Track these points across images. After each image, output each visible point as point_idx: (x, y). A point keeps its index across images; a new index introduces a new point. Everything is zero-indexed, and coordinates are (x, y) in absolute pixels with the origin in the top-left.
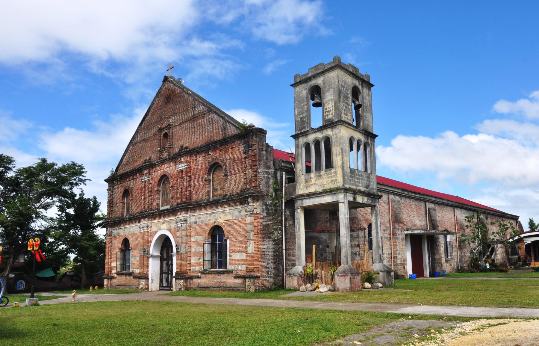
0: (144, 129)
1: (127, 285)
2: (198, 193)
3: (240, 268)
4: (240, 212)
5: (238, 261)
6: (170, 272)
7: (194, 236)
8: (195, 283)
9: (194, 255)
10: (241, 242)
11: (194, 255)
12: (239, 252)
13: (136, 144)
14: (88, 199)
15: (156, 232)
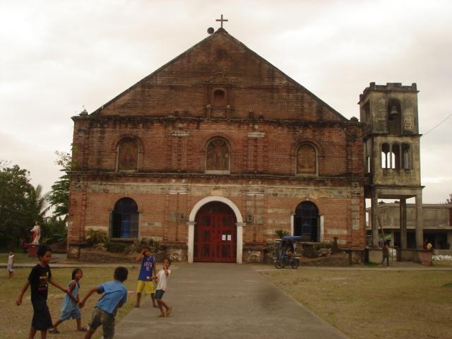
4: (340, 193)
7: (272, 208)
15: (202, 197)
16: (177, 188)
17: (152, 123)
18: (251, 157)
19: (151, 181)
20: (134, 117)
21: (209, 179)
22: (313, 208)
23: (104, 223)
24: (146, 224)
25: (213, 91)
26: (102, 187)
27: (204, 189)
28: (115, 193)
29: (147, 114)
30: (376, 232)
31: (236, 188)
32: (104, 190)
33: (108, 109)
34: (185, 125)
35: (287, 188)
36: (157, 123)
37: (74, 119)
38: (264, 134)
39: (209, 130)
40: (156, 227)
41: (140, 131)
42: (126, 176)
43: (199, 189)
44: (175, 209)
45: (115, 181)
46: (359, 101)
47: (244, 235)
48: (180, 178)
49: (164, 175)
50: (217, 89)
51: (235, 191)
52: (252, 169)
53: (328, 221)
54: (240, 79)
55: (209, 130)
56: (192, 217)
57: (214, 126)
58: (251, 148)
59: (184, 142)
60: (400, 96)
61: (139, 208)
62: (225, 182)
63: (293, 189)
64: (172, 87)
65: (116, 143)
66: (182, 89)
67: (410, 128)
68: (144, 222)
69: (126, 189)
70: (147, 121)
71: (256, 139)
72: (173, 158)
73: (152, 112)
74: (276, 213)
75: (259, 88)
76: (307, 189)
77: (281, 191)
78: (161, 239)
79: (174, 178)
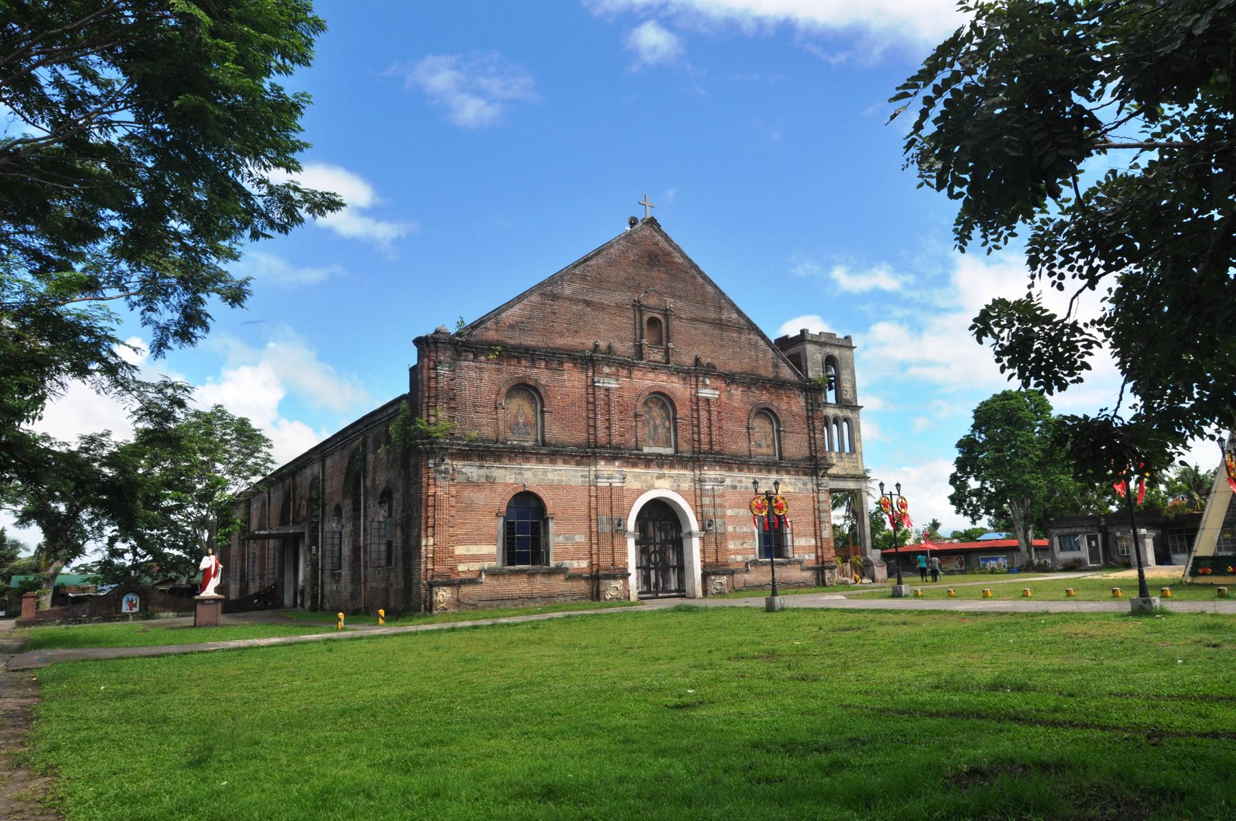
0: (584, 278)
1: (535, 595)
2: (736, 443)
3: (807, 557)
4: (805, 484)
5: (803, 548)
6: (652, 566)
7: (731, 507)
8: (741, 578)
9: (733, 537)
10: (807, 523)
11: (733, 537)
12: (805, 536)
13: (555, 297)
14: (975, 417)
15: (640, 492)
16: (608, 472)
17: (561, 363)
18: (704, 429)
19: (565, 462)
20: (536, 349)
21: (648, 461)
22: (533, 504)
23: (490, 540)
24: (561, 539)
25: (645, 318)
26: (483, 472)
27: (643, 478)
28: (506, 485)
29: (551, 345)
30: (283, 531)
31: (686, 476)
32: (487, 477)
34: (613, 369)
36: (568, 362)
38: (717, 392)
39: (647, 381)
40: (577, 543)
41: (541, 375)
42: (524, 453)
43: (637, 476)
44: (607, 510)
45: (506, 461)
47: (703, 551)
48: (611, 459)
49: (587, 453)
50: (651, 315)
51: (685, 482)
52: (705, 447)
54: (679, 304)
55: (647, 381)
56: (631, 524)
57: (651, 375)
58: (703, 414)
59: (614, 398)
60: (836, 352)
61: (549, 511)
62: (672, 466)
64: (588, 303)
65: (504, 390)
66: (601, 307)
67: (848, 397)
68: (558, 535)
69: (526, 476)
70: (555, 357)
71: (708, 400)
72: (599, 423)
73: (560, 342)
74: (736, 516)
75: (704, 321)
78: (584, 564)
79: (604, 458)
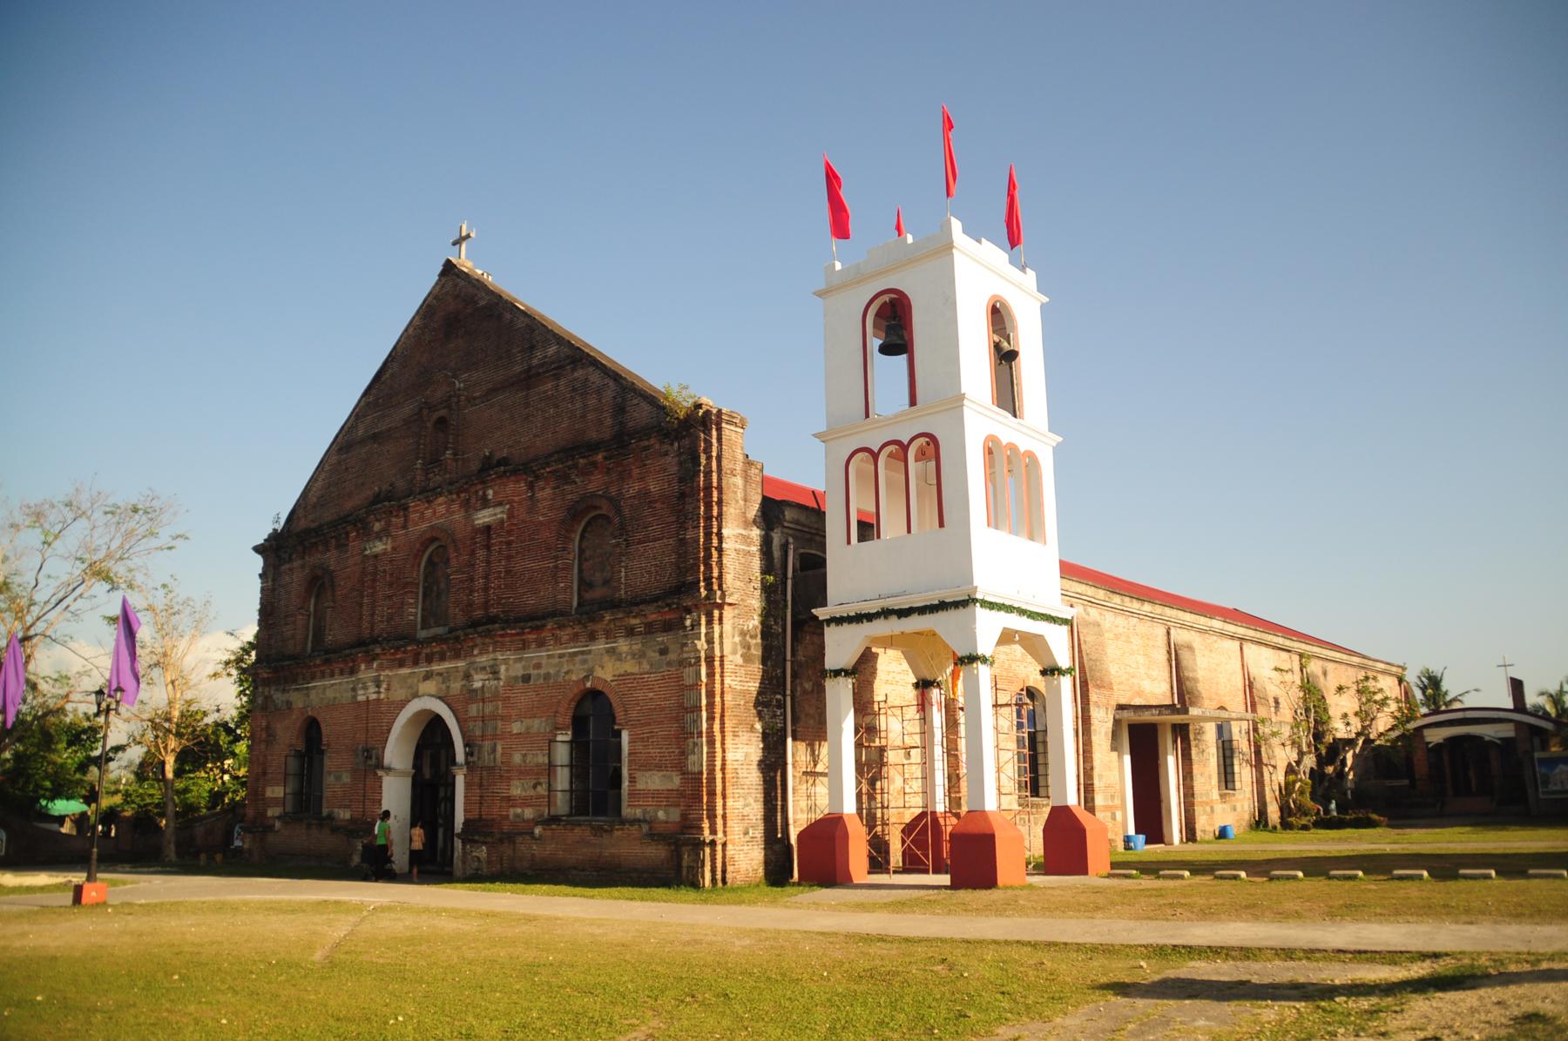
7: (520, 718)
33: (586, 560)
35: (549, 657)
37: (257, 549)
46: (261, 572)
53: (639, 746)
63: (561, 656)
76: (589, 652)
77: (538, 666)
